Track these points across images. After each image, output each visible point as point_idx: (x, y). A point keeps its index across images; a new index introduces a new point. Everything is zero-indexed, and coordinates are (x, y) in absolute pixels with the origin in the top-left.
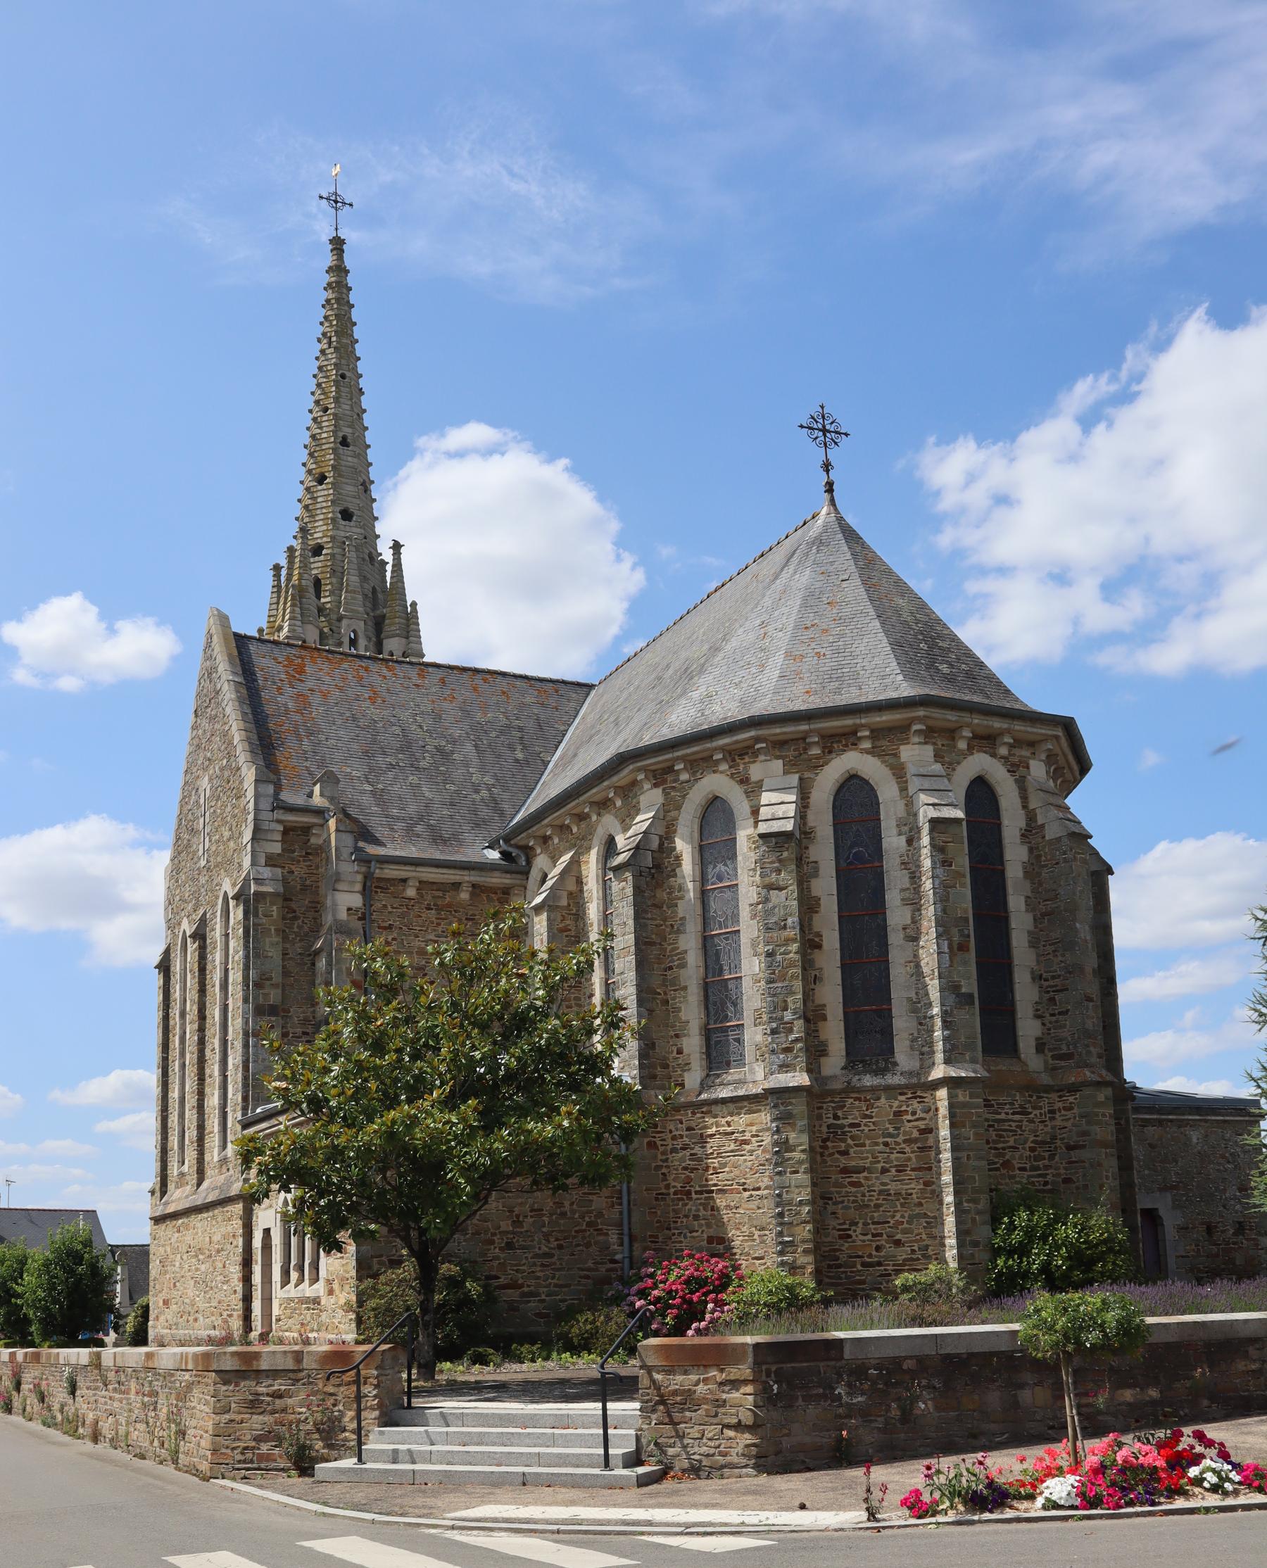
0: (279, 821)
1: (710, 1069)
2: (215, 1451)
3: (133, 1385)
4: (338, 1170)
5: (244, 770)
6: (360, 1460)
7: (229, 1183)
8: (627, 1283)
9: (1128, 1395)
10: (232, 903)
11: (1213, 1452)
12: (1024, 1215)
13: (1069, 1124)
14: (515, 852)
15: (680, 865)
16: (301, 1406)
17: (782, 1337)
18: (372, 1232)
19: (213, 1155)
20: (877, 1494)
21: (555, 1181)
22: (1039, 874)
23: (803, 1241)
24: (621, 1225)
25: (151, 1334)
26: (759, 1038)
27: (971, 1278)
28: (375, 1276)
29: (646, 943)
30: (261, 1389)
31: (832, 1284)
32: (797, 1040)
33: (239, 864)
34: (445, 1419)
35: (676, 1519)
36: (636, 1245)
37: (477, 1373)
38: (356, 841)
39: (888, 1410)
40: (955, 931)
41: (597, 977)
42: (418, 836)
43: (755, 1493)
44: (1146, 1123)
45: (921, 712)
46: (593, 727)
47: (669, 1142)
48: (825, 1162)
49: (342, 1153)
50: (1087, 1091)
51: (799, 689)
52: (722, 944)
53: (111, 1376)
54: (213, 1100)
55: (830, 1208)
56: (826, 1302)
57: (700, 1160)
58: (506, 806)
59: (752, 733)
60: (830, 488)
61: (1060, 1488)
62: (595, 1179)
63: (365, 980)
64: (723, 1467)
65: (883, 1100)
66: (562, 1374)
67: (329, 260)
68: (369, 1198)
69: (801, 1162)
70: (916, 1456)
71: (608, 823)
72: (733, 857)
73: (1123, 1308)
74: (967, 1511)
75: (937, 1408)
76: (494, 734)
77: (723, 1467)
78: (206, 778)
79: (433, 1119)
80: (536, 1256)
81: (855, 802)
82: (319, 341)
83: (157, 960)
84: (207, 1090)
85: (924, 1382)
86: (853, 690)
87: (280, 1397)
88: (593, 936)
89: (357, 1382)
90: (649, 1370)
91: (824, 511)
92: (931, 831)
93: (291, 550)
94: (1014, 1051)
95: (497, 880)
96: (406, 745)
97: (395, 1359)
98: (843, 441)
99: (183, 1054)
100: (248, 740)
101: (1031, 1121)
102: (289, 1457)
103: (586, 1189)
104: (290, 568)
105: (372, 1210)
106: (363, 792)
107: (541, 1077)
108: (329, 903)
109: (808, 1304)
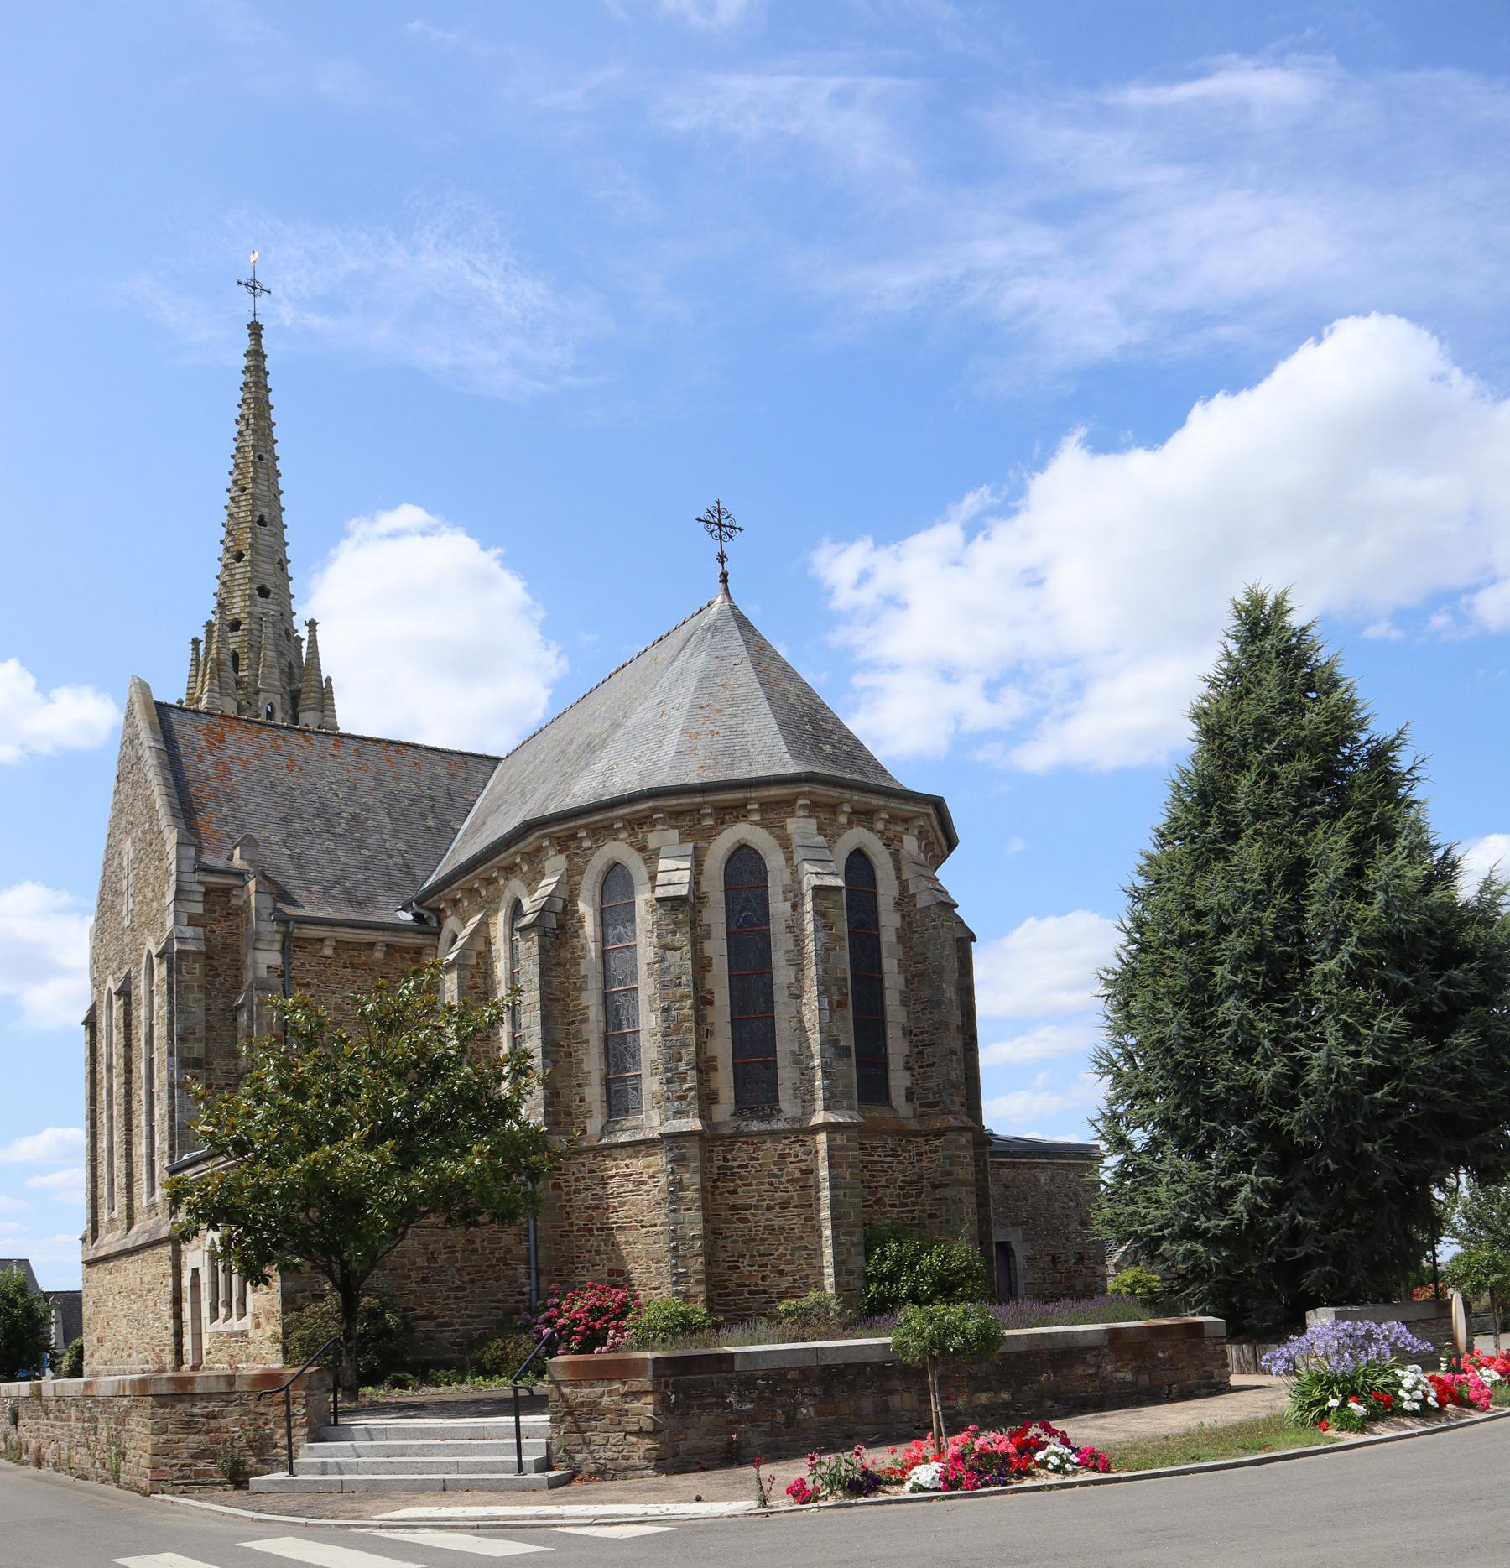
0: (200, 883)
1: (610, 1116)
2: (154, 1469)
3: (73, 1413)
4: (262, 1209)
5: (166, 834)
6: (291, 1473)
7: (158, 1227)
8: (535, 1312)
9: (983, 1398)
10: (156, 961)
11: (1057, 1440)
12: (894, 1246)
13: (934, 1165)
14: (426, 914)
15: (582, 927)
16: (233, 1425)
17: (678, 1353)
18: (297, 1265)
19: (142, 1201)
20: (766, 1486)
21: (468, 1218)
22: (910, 939)
23: (696, 1272)
24: (529, 1260)
25: (86, 1370)
26: (655, 1087)
27: (847, 1303)
28: (300, 1309)
29: (551, 999)
30: (196, 1411)
31: (722, 1311)
32: (690, 1089)
33: (163, 923)
34: (370, 1434)
35: (585, 1513)
36: (543, 1278)
37: (397, 1395)
38: (275, 902)
39: (774, 1416)
40: (834, 990)
41: (505, 1032)
42: (334, 898)
43: (656, 1490)
44: (1001, 1165)
45: (806, 788)
46: (500, 797)
47: (573, 1183)
48: (715, 1200)
49: (267, 1192)
50: (951, 1136)
51: (695, 763)
52: (621, 1001)
53: (52, 1405)
54: (140, 1149)
55: (721, 1242)
56: (717, 1326)
57: (601, 1199)
58: (418, 871)
59: (650, 804)
60: (724, 578)
61: (925, 1474)
62: (505, 1215)
63: (286, 1031)
64: (626, 1469)
65: (768, 1144)
66: (476, 1395)
67: (247, 343)
68: (294, 1235)
69: (693, 1201)
70: (800, 1455)
71: (514, 887)
72: (632, 919)
73: (982, 1317)
74: (845, 1496)
75: (816, 1412)
76: (406, 803)
77: (626, 1469)
78: (129, 842)
79: (353, 1159)
80: (450, 1289)
81: (745, 869)
82: (237, 422)
83: (83, 1016)
84: (135, 1140)
85: (806, 1391)
86: (744, 766)
87: (215, 1417)
88: (502, 991)
89: (287, 1402)
90: (558, 1384)
91: (719, 600)
92: (814, 898)
93: (209, 624)
94: (886, 1099)
95: (409, 940)
96: (323, 812)
97: (321, 1380)
98: (737, 534)
99: (110, 1106)
100: (170, 804)
101: (901, 1163)
102: (225, 1473)
103: (495, 1226)
104: (209, 642)
105: (297, 1246)
106: (282, 856)
107: (455, 1121)
108: (249, 961)
109: (700, 1328)
